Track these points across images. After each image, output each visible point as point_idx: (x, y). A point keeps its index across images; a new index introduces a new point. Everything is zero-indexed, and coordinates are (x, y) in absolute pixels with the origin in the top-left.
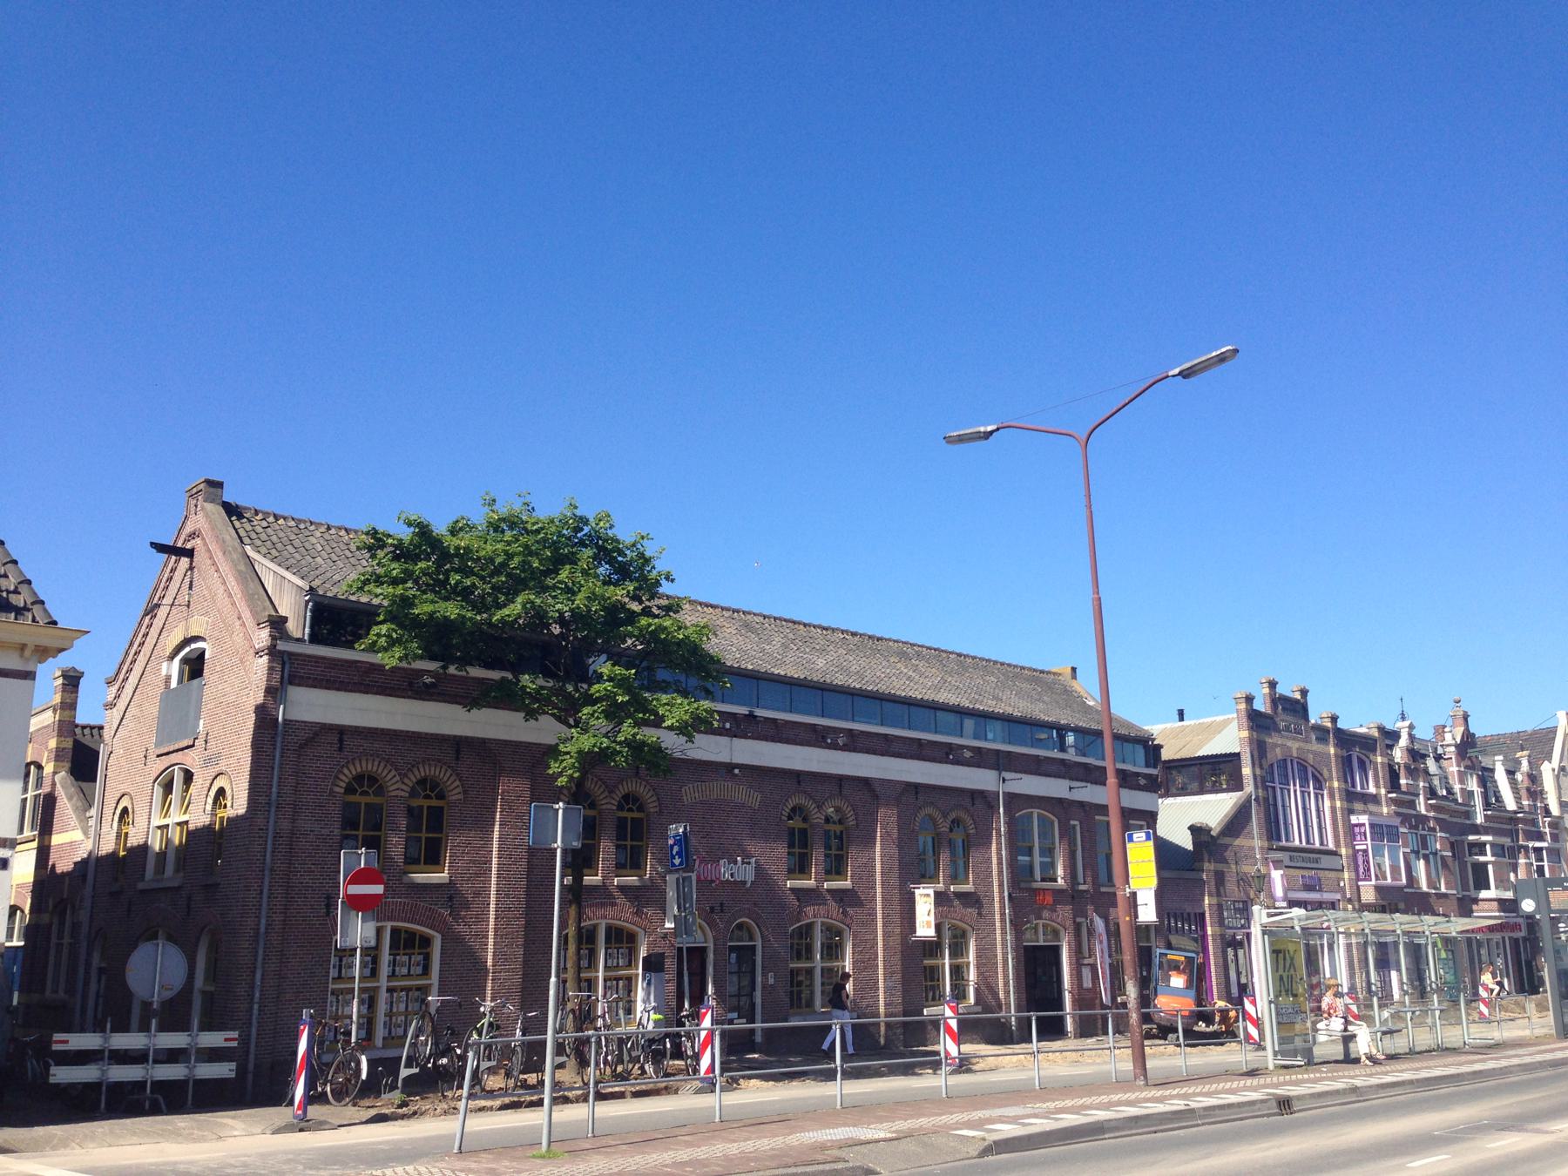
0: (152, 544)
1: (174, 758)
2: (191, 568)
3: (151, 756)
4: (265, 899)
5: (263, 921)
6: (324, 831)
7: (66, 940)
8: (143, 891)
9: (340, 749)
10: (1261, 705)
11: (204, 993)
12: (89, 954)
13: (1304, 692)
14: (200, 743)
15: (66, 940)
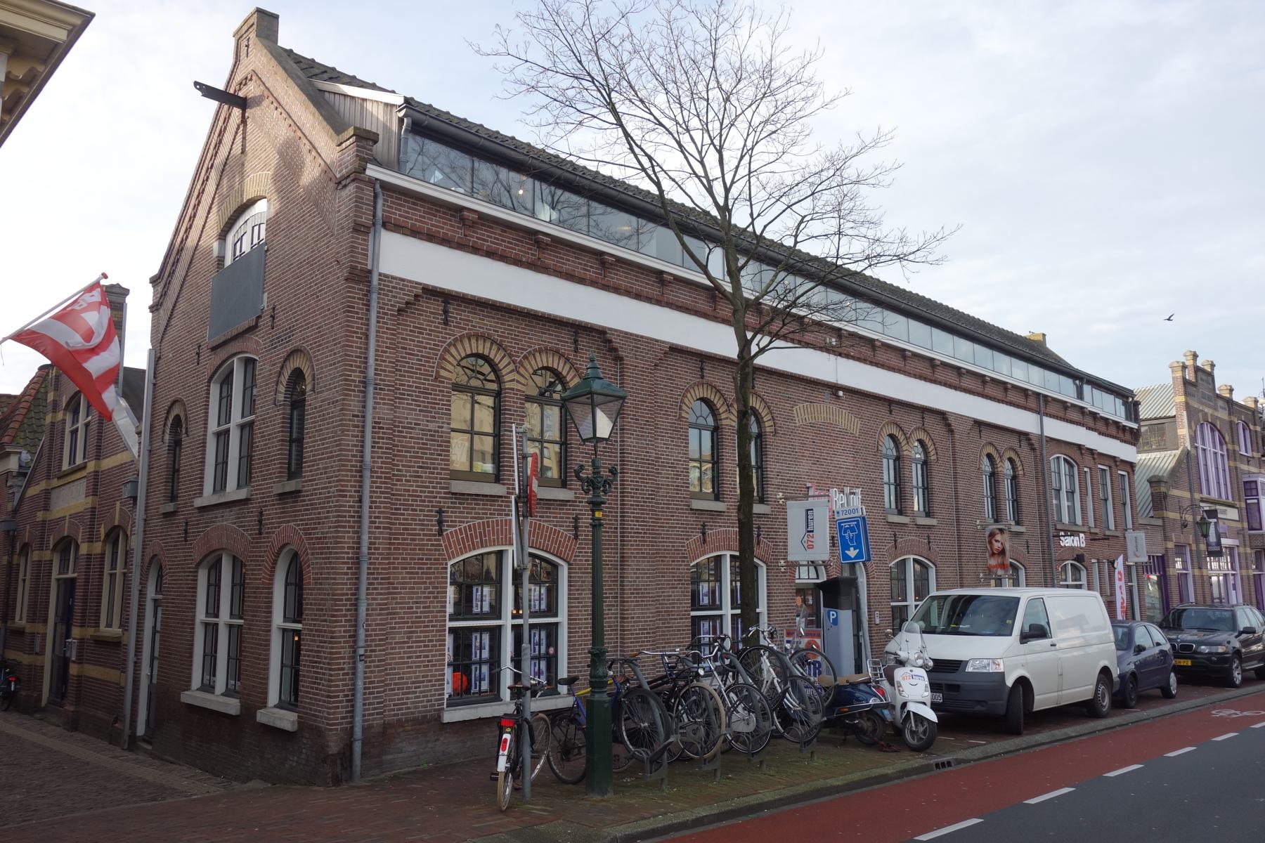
0: (197, 84)
1: (231, 348)
2: (244, 121)
3: (205, 353)
4: (366, 510)
5: (365, 537)
6: (432, 426)
7: (119, 570)
8: (203, 509)
9: (446, 322)
10: (1190, 375)
11: (231, 626)
12: (143, 584)
13: (1213, 366)
14: (266, 320)
15: (119, 570)
